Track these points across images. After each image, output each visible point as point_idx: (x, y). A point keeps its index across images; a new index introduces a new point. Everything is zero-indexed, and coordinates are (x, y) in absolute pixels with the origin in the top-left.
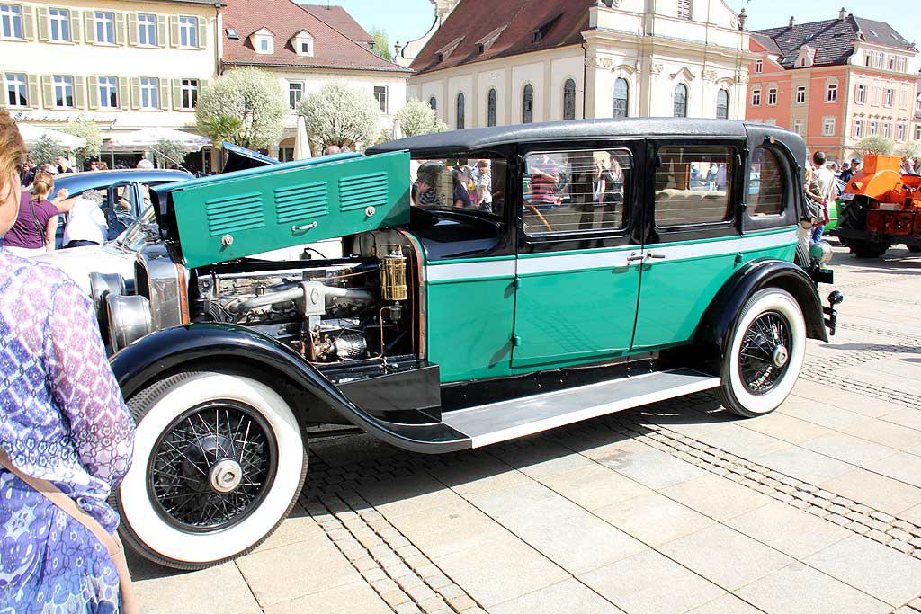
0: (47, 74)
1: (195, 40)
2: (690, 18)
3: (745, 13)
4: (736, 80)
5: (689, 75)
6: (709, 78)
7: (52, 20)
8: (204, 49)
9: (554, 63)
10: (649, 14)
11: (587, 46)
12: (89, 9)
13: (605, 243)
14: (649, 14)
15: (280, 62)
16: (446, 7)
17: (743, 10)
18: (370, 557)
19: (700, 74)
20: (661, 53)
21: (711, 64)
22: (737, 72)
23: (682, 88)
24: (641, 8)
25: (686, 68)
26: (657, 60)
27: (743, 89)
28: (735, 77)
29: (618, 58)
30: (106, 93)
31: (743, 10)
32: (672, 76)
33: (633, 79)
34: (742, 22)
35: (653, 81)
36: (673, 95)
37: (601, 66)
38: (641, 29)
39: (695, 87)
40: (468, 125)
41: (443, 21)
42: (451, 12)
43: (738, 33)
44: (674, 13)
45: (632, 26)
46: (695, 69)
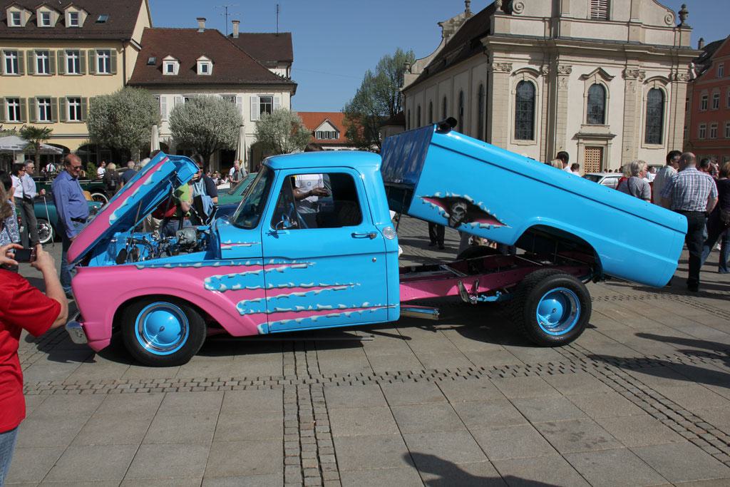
0: (32, 96)
1: (110, 68)
2: (608, 19)
3: (686, 9)
4: (673, 79)
5: (607, 77)
6: (632, 77)
7: (38, 59)
8: (115, 74)
9: (475, 69)
10: (554, 20)
11: (489, 52)
12: (62, 49)
13: (141, 331)
14: (554, 20)
15: (186, 81)
16: (451, 28)
17: (683, 6)
18: (646, 331)
19: (621, 74)
20: (571, 52)
21: (637, 62)
22: (674, 71)
23: (598, 89)
24: (548, 13)
25: (600, 68)
26: (563, 61)
27: (683, 88)
28: (670, 75)
29: (520, 62)
30: (44, 109)
31: (683, 6)
32: (584, 77)
33: (540, 82)
34: (682, 19)
35: (561, 84)
36: (586, 95)
37: (500, 70)
38: (548, 31)
39: (616, 89)
40: (422, 126)
41: (448, 41)
42: (456, 33)
43: (674, 31)
44: (587, 13)
45: (538, 30)
46: (614, 70)
